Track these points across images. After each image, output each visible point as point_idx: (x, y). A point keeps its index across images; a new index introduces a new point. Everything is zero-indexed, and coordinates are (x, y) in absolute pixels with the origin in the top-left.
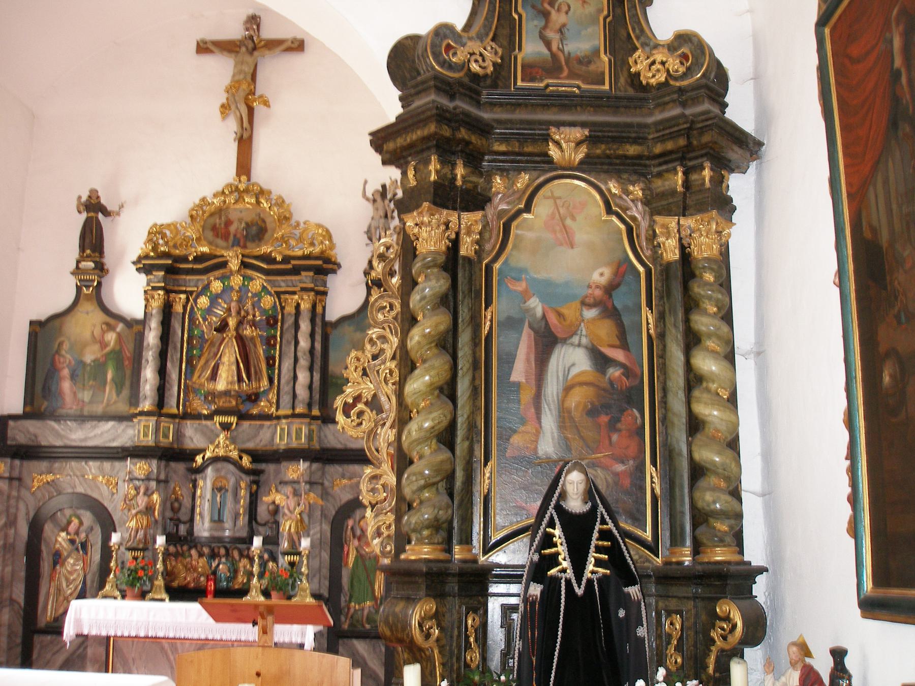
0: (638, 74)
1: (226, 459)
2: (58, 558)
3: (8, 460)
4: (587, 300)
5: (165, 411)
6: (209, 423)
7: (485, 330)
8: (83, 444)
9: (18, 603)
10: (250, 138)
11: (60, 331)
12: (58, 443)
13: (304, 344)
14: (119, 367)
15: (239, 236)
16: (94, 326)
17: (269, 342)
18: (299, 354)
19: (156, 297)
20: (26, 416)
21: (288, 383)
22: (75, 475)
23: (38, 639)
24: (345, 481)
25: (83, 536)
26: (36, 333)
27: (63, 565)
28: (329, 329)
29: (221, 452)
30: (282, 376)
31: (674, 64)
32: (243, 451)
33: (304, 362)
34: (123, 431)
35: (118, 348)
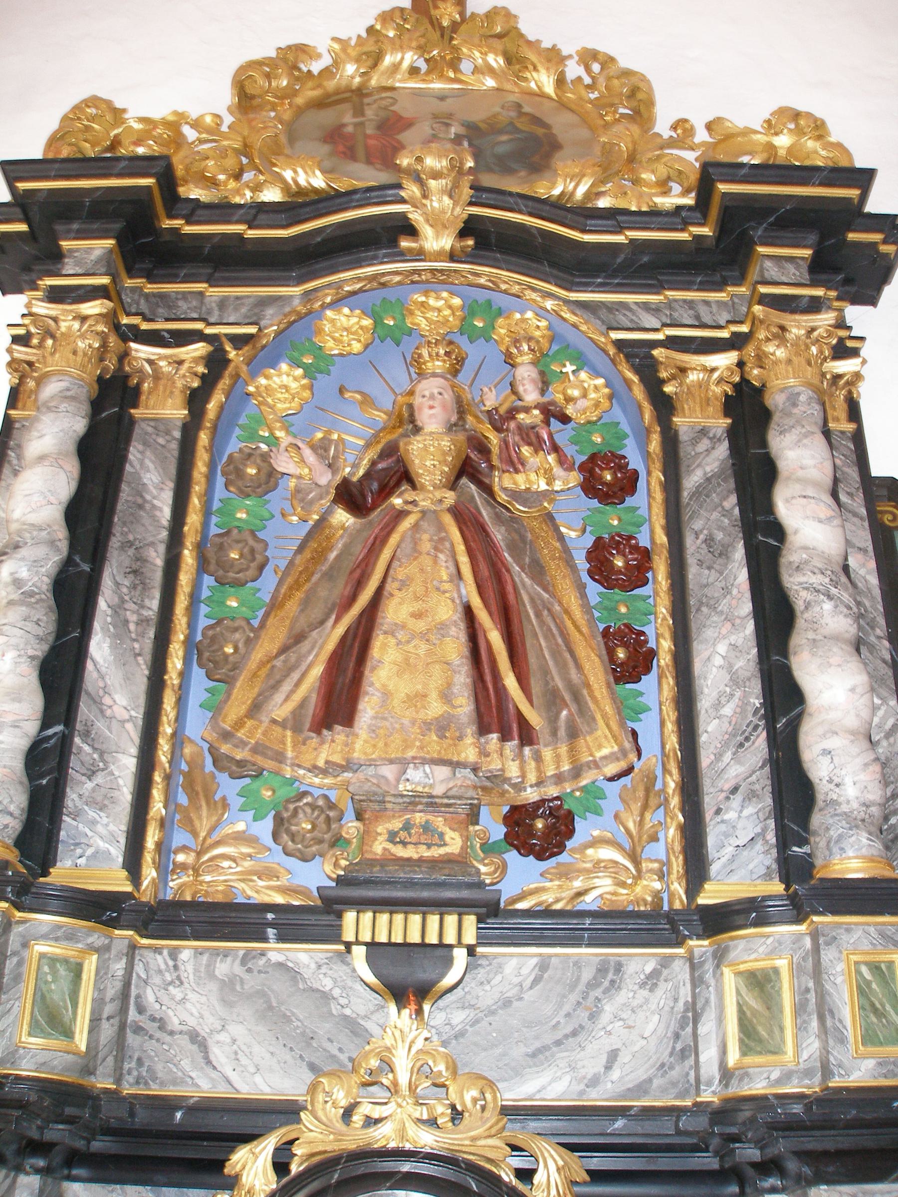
30: (704, 704)
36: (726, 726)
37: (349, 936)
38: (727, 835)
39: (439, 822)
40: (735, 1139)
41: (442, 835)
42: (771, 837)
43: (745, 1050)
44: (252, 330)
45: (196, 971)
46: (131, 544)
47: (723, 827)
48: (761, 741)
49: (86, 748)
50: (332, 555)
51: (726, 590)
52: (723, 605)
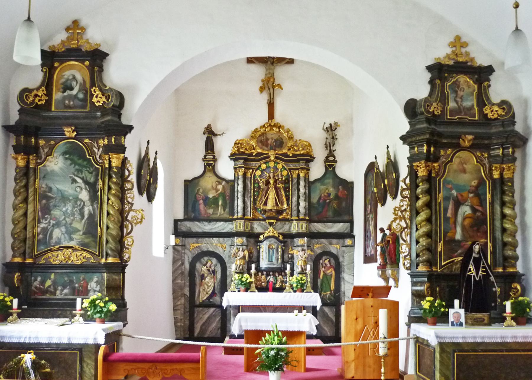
0: (487, 114)
1: (273, 237)
2: (203, 277)
3: (181, 238)
4: (470, 191)
5: (246, 217)
6: (263, 222)
7: (438, 201)
8: (211, 231)
9: (187, 295)
10: (273, 103)
11: (197, 184)
12: (200, 231)
13: (302, 190)
14: (224, 200)
15: (272, 145)
16: (213, 182)
17: (286, 189)
18: (301, 195)
19: (241, 171)
20: (185, 220)
21: (295, 206)
23: (196, 309)
24: (318, 246)
25: (213, 268)
26: (187, 185)
27: (205, 280)
28: (310, 184)
29: (271, 234)
31: (500, 112)
32: (279, 233)
33: (302, 198)
35: (223, 192)
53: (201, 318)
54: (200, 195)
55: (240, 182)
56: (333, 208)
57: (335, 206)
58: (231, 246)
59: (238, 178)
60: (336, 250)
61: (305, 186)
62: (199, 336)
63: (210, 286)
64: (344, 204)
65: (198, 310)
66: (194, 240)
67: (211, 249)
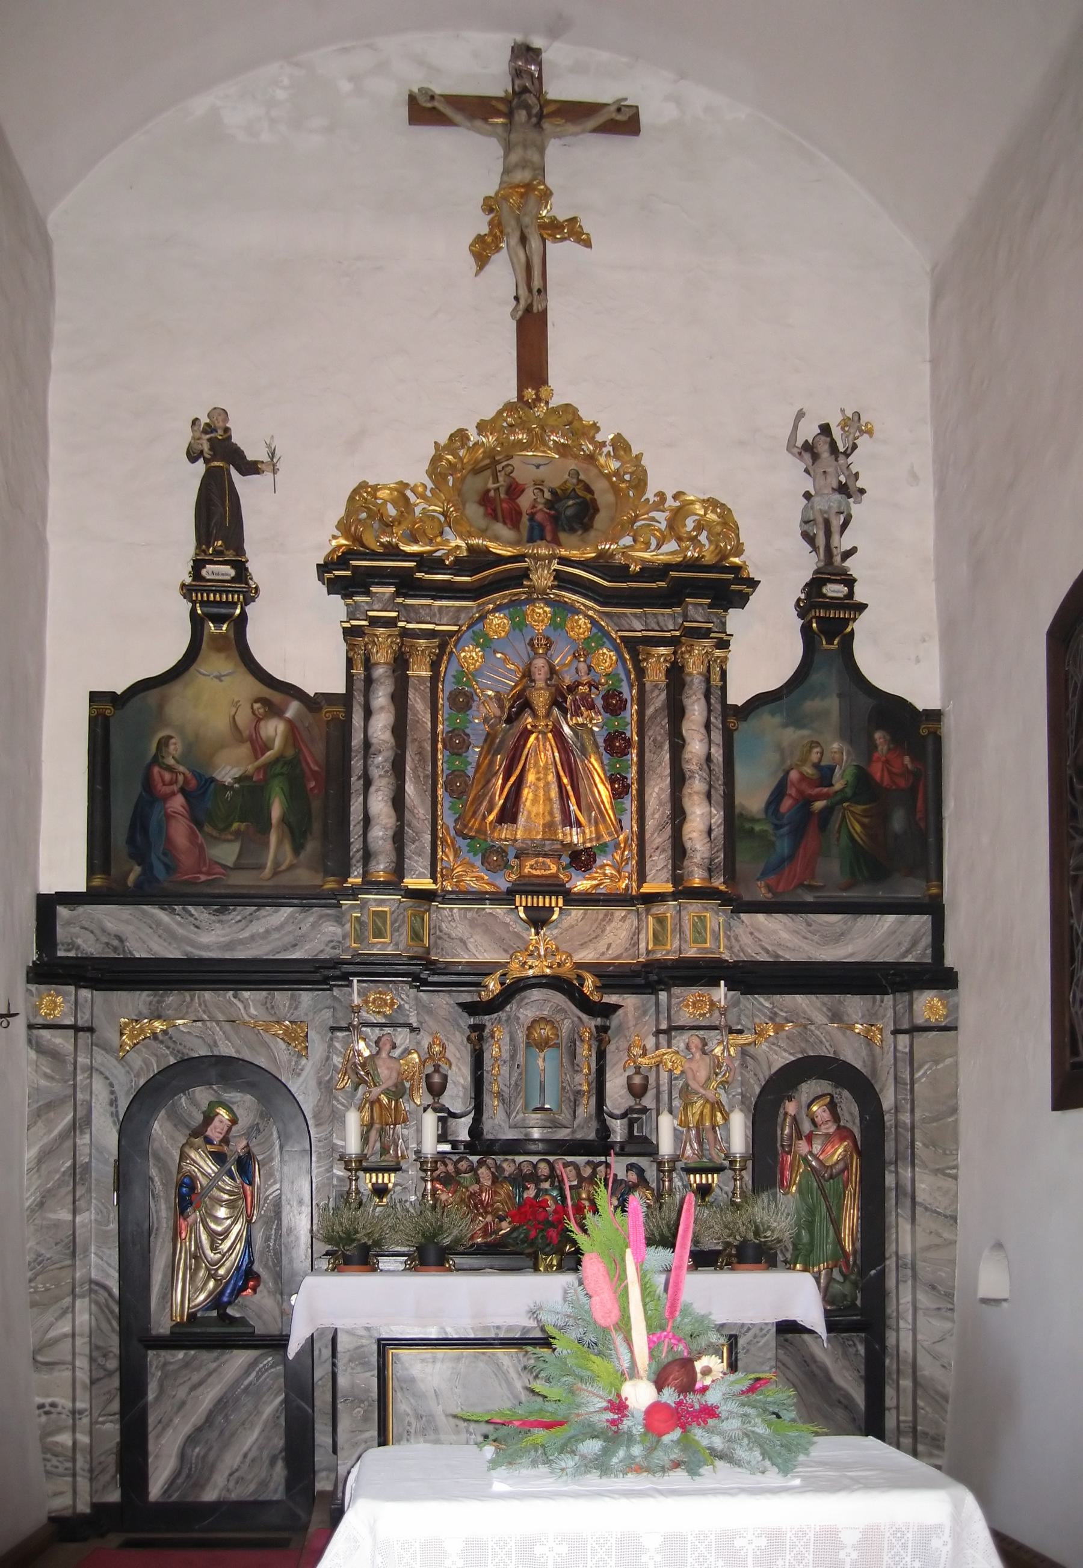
6: (500, 910)
8: (228, 955)
9: (105, 1288)
10: (544, 313)
13: (695, 747)
14: (296, 795)
15: (539, 517)
16: (236, 705)
21: (661, 828)
22: (212, 1019)
26: (106, 719)
30: (648, 813)
34: (313, 925)
35: (290, 753)
36: (656, 822)
37: (518, 904)
38: (653, 866)
39: (548, 861)
40: (651, 973)
41: (549, 866)
42: (670, 867)
43: (655, 944)
44: (456, 628)
45: (460, 917)
46: (416, 740)
47: (652, 863)
48: (669, 828)
49: (411, 832)
50: (498, 740)
51: (660, 764)
52: (658, 770)
53: (183, 1404)
54: (170, 769)
55: (381, 698)
56: (844, 840)
57: (858, 828)
58: (333, 1029)
59: (369, 681)
60: (864, 1053)
61: (708, 726)
62: (175, 1497)
63: (226, 1233)
64: (898, 821)
65: (165, 1364)
66: (141, 999)
67: (226, 1049)
